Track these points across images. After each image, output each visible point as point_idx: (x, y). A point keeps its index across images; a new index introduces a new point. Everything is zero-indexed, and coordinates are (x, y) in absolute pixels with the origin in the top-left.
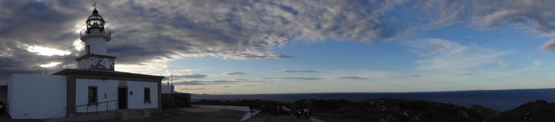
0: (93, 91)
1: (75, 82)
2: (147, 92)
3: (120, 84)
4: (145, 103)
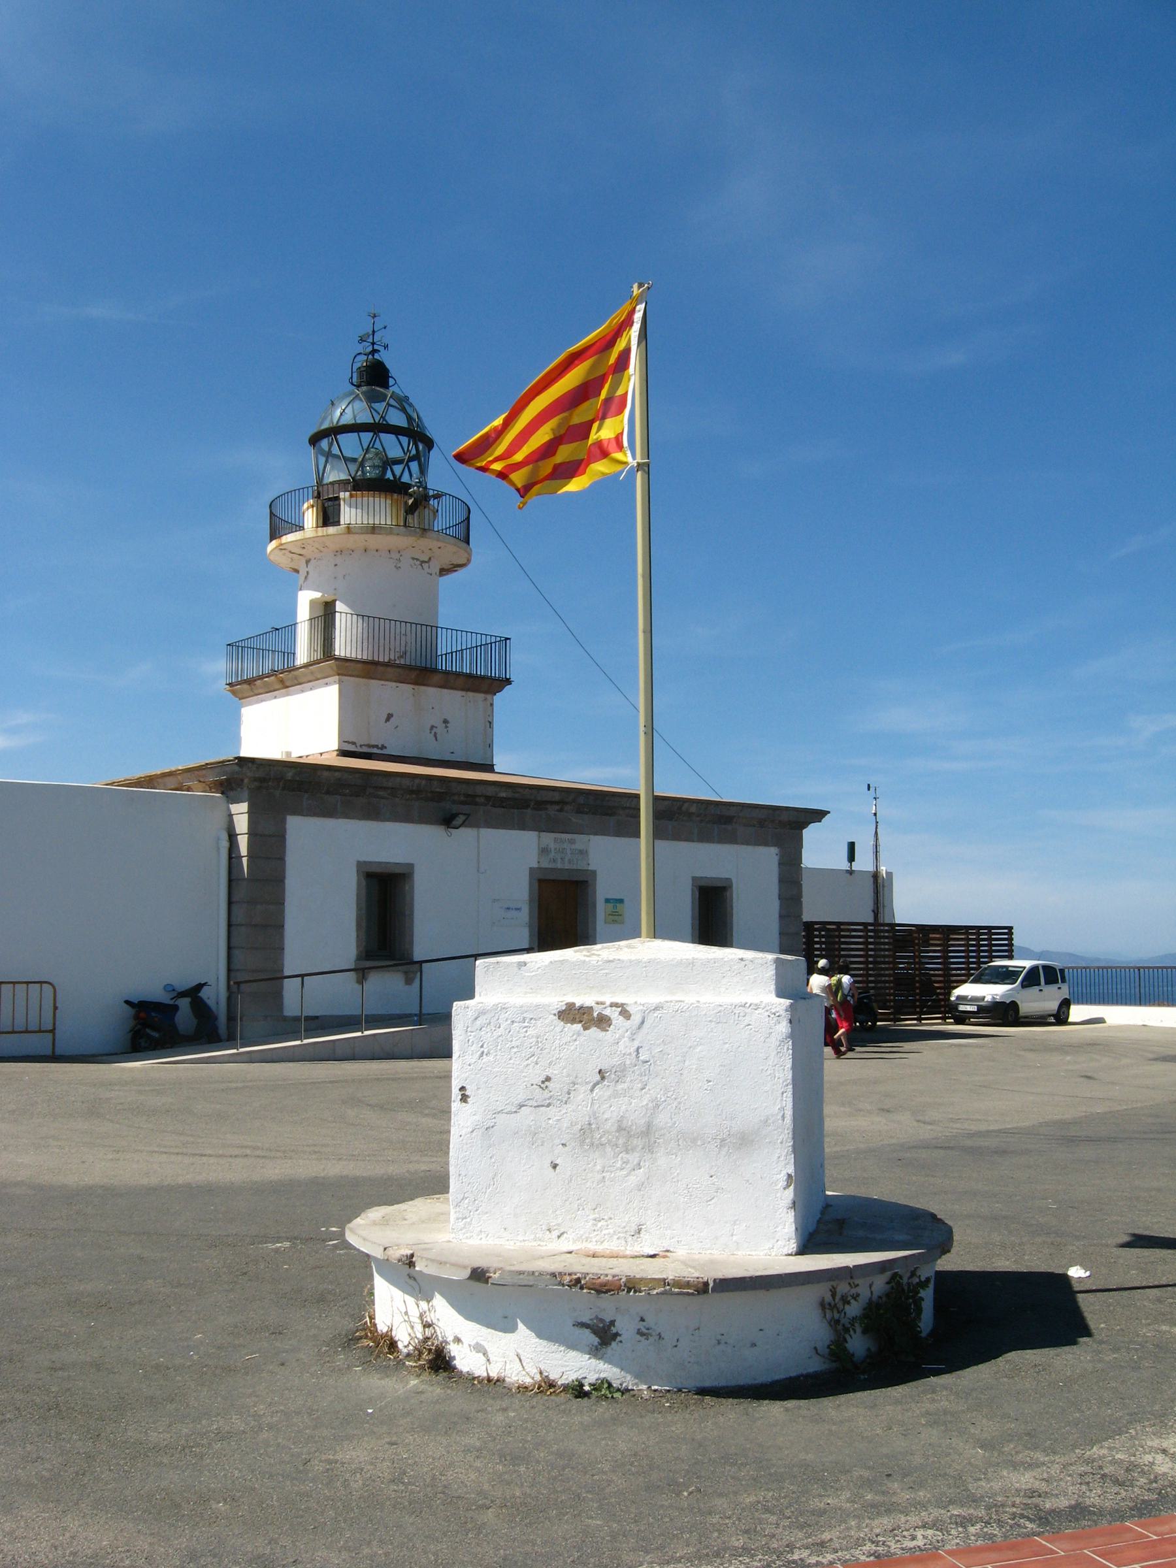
3: (544, 851)
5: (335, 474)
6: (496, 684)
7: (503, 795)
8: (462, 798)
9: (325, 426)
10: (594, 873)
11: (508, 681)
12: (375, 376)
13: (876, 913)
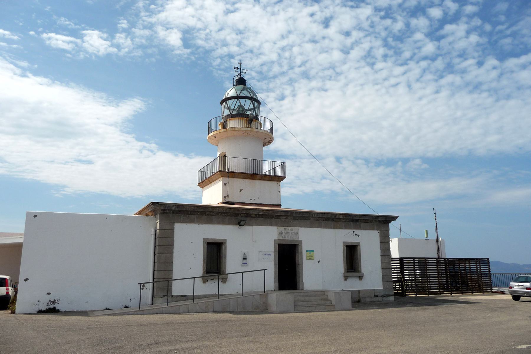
0: (215, 252)
1: (173, 230)
2: (352, 252)
3: (280, 233)
4: (346, 278)
5: (227, 112)
6: (280, 178)
7: (261, 213)
8: (246, 215)
9: (224, 98)
10: (301, 241)
11: (285, 177)
12: (241, 81)
13: (439, 255)
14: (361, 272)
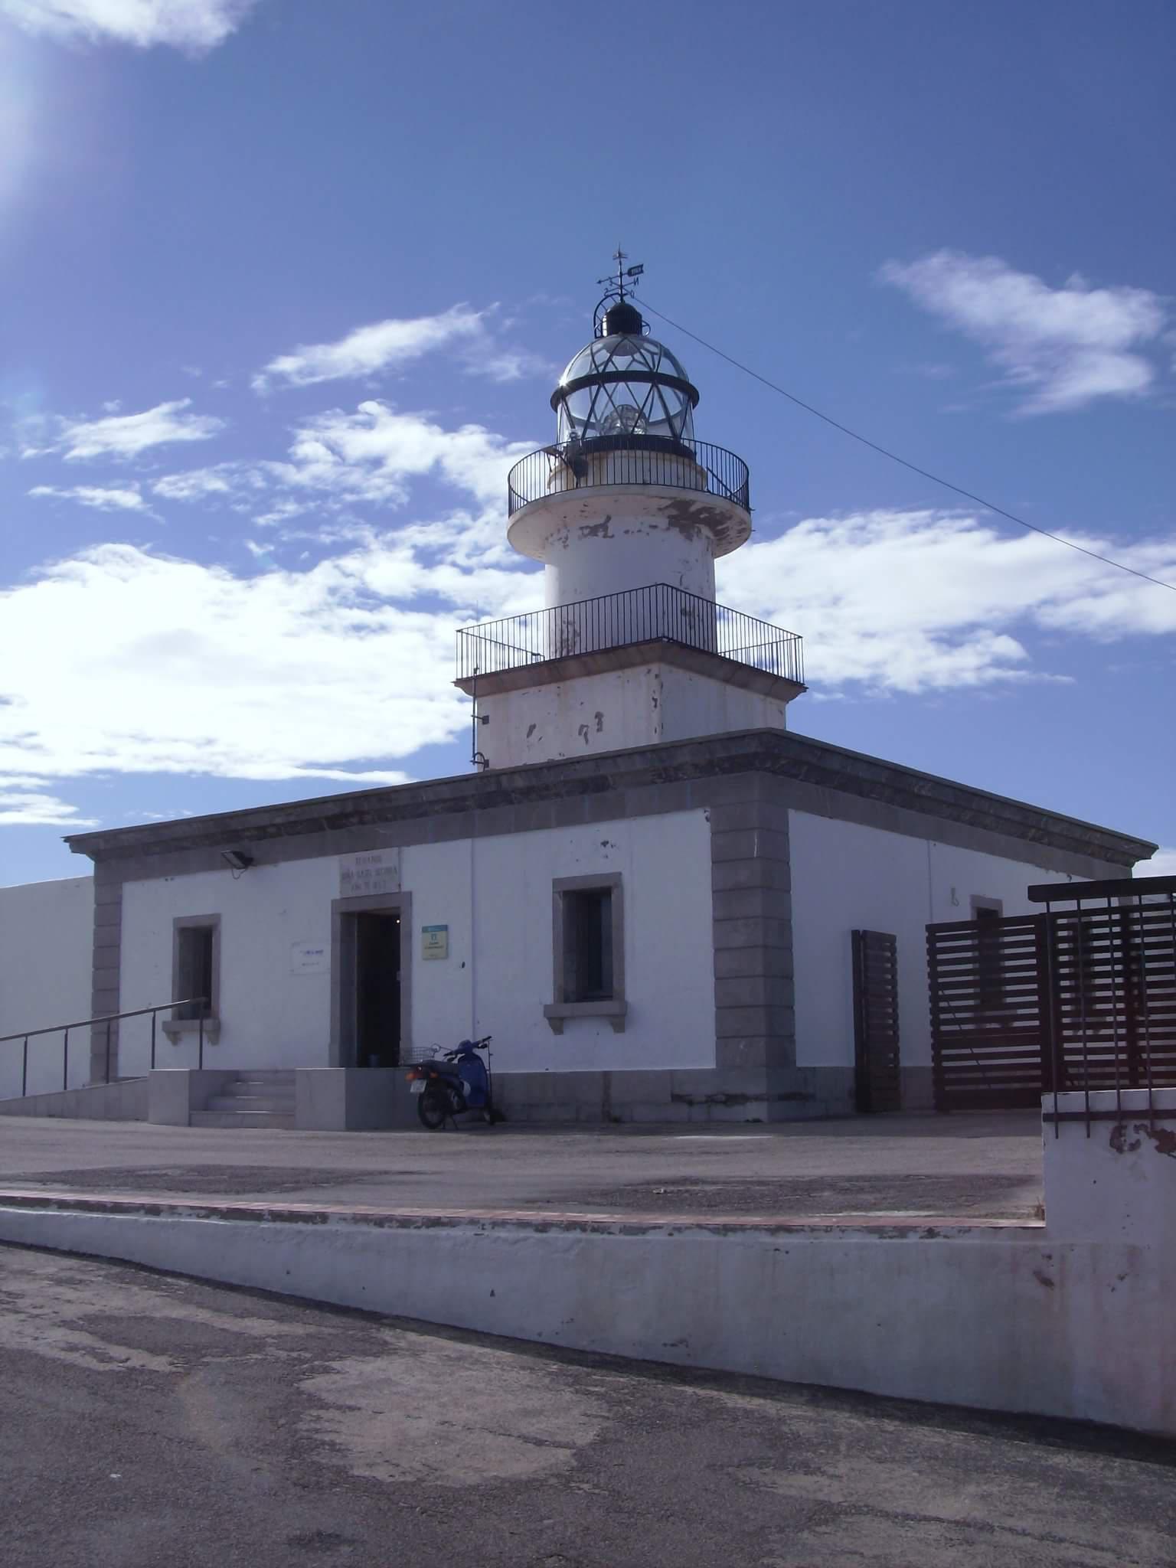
3: (346, 877)
11: (459, 683)
14: (621, 998)
